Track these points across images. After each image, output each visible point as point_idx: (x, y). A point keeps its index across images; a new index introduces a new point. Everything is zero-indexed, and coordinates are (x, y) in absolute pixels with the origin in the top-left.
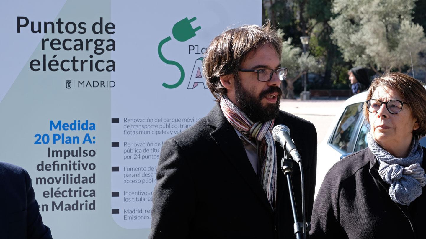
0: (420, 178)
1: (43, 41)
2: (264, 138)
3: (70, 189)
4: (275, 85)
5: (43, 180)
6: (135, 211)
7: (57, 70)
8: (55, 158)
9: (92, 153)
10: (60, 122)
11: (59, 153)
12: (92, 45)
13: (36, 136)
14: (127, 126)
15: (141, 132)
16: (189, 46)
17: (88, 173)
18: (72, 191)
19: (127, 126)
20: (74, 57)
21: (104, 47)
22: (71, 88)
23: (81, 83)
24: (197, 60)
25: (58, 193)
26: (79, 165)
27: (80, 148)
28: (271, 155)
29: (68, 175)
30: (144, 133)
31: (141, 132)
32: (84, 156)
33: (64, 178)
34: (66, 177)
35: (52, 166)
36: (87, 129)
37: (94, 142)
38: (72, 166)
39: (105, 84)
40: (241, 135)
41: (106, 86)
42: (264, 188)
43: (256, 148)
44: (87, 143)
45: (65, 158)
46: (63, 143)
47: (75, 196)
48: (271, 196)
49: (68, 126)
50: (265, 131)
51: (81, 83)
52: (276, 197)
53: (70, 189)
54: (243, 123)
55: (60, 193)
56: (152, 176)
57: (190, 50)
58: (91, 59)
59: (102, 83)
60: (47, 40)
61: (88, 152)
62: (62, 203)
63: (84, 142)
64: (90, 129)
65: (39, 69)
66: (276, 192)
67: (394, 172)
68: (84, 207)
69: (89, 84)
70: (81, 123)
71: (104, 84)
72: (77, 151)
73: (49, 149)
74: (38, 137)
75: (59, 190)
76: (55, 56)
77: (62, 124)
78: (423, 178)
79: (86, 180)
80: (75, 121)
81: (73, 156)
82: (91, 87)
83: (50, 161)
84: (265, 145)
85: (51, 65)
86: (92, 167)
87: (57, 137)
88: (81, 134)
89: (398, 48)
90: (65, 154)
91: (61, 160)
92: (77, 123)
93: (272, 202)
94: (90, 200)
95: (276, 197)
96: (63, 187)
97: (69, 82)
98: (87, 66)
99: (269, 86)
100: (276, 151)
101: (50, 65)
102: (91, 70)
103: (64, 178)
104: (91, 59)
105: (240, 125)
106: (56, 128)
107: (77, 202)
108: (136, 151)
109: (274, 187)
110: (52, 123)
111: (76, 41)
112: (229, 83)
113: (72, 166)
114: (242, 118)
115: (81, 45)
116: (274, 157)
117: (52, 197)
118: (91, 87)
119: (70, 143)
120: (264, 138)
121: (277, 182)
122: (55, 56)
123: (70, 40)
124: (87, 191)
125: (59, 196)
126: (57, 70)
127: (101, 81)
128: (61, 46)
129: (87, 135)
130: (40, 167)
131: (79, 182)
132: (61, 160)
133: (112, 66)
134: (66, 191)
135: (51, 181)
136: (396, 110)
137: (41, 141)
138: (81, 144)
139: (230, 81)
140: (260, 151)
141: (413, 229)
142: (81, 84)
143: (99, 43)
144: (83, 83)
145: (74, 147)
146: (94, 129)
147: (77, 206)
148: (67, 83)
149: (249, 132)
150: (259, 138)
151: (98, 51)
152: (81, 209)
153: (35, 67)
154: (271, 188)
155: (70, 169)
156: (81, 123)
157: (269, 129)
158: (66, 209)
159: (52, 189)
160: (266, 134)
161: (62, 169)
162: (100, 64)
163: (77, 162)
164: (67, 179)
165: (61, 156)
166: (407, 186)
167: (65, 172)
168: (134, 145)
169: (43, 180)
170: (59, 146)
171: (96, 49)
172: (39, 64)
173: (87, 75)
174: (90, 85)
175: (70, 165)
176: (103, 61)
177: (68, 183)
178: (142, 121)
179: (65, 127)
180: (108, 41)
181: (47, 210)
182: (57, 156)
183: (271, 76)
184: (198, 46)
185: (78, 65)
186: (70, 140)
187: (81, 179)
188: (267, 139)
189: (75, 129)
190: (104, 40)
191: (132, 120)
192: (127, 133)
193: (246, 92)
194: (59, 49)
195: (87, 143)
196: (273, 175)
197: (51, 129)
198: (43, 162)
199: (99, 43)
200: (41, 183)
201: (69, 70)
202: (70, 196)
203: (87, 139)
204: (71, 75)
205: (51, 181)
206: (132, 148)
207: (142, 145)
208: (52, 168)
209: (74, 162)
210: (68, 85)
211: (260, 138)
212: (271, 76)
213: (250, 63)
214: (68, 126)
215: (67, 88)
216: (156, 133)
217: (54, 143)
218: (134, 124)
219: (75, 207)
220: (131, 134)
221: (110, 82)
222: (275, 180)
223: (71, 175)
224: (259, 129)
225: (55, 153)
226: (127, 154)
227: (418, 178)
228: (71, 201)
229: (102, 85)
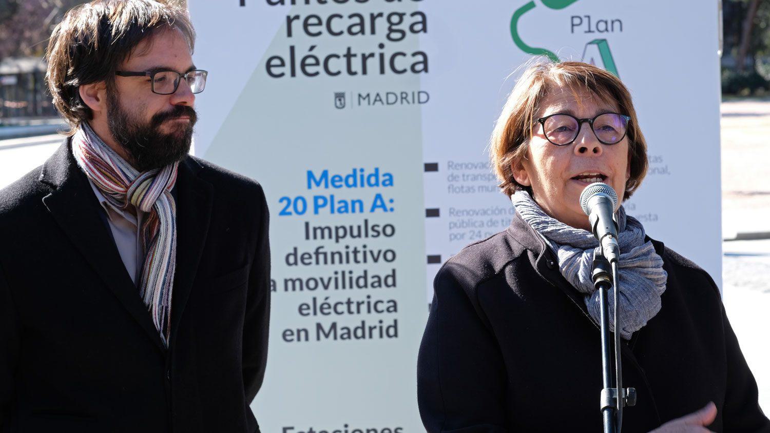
0: (656, 277)
1: (290, 20)
2: (154, 207)
3: (349, 299)
4: (185, 102)
5: (297, 283)
7: (317, 74)
8: (319, 242)
9: (389, 230)
10: (325, 174)
11: (326, 232)
12: (382, 25)
13: (281, 200)
14: (454, 178)
15: (481, 188)
16: (573, 18)
17: (382, 269)
18: (352, 303)
19: (454, 178)
20: (349, 49)
21: (405, 26)
24: (590, 46)
25: (326, 306)
26: (365, 253)
27: (366, 222)
28: (166, 239)
29: (343, 273)
30: (487, 189)
31: (481, 188)
32: (373, 236)
33: (336, 279)
34: (340, 276)
35: (314, 256)
36: (377, 184)
37: (392, 210)
38: (351, 256)
40: (104, 200)
42: (147, 301)
43: (136, 224)
44: (379, 211)
45: (337, 241)
46: (332, 211)
47: (359, 312)
48: (161, 317)
49: (341, 180)
50: (155, 193)
52: (169, 317)
53: (349, 299)
54: (113, 178)
55: (329, 307)
57: (573, 25)
58: (382, 51)
60: (297, 17)
61: (380, 229)
62: (334, 326)
63: (372, 210)
64: (384, 184)
65: (282, 75)
66: (170, 308)
68: (376, 332)
69: (378, 99)
70: (366, 174)
72: (359, 227)
73: (307, 224)
74: (285, 203)
75: (328, 301)
76: (312, 48)
77: (330, 176)
78: (662, 276)
79: (379, 282)
80: (355, 171)
81: (352, 236)
82: (383, 103)
83: (310, 246)
84: (156, 219)
85: (304, 66)
86: (389, 256)
87: (321, 202)
88: (367, 194)
90: (338, 233)
91: (330, 246)
92: (359, 174)
93: (162, 327)
94: (388, 319)
95: (169, 317)
96: (336, 295)
97: (340, 96)
98: (373, 64)
99: (173, 105)
100: (175, 231)
101: (303, 65)
102: (382, 71)
103: (336, 279)
104: (382, 51)
105: (108, 182)
106: (318, 184)
107: (363, 323)
108: (473, 224)
109: (167, 300)
110: (310, 175)
111: (351, 17)
112: (98, 100)
113: (351, 256)
114: (114, 168)
115: (360, 26)
116: (172, 242)
117: (315, 313)
118: (383, 103)
119: (347, 211)
120: (154, 207)
121: (173, 289)
122: (312, 48)
123: (340, 16)
124: (382, 302)
125: (329, 313)
126: (317, 74)
128: (323, 28)
129: (378, 196)
130: (292, 259)
131: (366, 286)
132: (330, 246)
133: (423, 63)
134: (341, 303)
135: (312, 284)
137: (291, 209)
138: (367, 214)
139: (99, 96)
140: (144, 229)
142: (364, 99)
143: (395, 19)
145: (353, 220)
146: (391, 184)
147: (363, 332)
149: (125, 196)
150: (144, 206)
151: (395, 35)
152: (371, 336)
153: (275, 71)
154: (161, 300)
155: (348, 261)
156: (366, 174)
157: (163, 189)
158: (342, 337)
159: (315, 300)
160: (158, 198)
161: (333, 262)
162: (398, 59)
163: (360, 249)
164: (343, 281)
165: (330, 237)
166: (632, 292)
167: (338, 267)
168: (468, 213)
169: (297, 283)
170: (325, 218)
171: (391, 30)
172: (283, 64)
173: (375, 81)
174: (380, 100)
175: (347, 254)
176: (404, 54)
177: (344, 287)
179: (336, 181)
180: (413, 15)
181: (307, 339)
182: (323, 237)
183: (177, 85)
184: (589, 17)
185: (356, 64)
186: (345, 207)
187: (370, 281)
188: (159, 207)
189: (355, 185)
190: (404, 14)
191: (464, 166)
192: (454, 190)
193: (127, 116)
194: (319, 34)
195: (379, 211)
196: (166, 275)
197: (309, 187)
198: (295, 249)
199: (395, 19)
200: (294, 289)
201: (339, 73)
202: (350, 312)
203: (379, 203)
204: (344, 83)
205: (312, 284)
206: (466, 218)
207: (485, 212)
208: (313, 260)
209: (355, 249)
210: (338, 103)
211: (146, 207)
212: (177, 85)
213: (137, 62)
214: (341, 180)
215: (337, 107)
217: (316, 212)
218: (467, 172)
219: (359, 333)
222: (169, 286)
223: (351, 272)
224: (144, 189)
225: (319, 232)
226: (455, 231)
227: (653, 277)
228: (353, 321)
229: (404, 100)
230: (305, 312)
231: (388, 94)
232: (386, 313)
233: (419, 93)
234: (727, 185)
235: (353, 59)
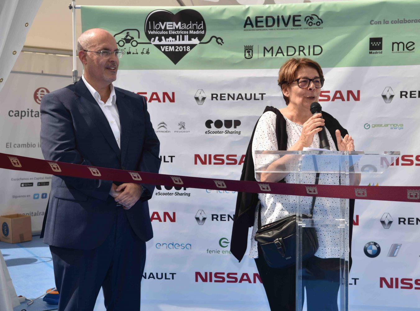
22: (252, 57)
23: (268, 50)
51: (268, 50)
59: (302, 49)
67: (124, 195)
71: (304, 51)
118: (284, 55)
136: (349, 138)
142: (268, 51)
144: (271, 50)
148: (246, 51)
174: (282, 52)
178: (28, 179)
198: (21, 118)
200: (24, 147)
210: (247, 54)
221: (314, 46)
229: (301, 53)
231: (288, 47)
232: (17, 148)
233: (314, 46)
234: (148, 269)
235: (33, 113)
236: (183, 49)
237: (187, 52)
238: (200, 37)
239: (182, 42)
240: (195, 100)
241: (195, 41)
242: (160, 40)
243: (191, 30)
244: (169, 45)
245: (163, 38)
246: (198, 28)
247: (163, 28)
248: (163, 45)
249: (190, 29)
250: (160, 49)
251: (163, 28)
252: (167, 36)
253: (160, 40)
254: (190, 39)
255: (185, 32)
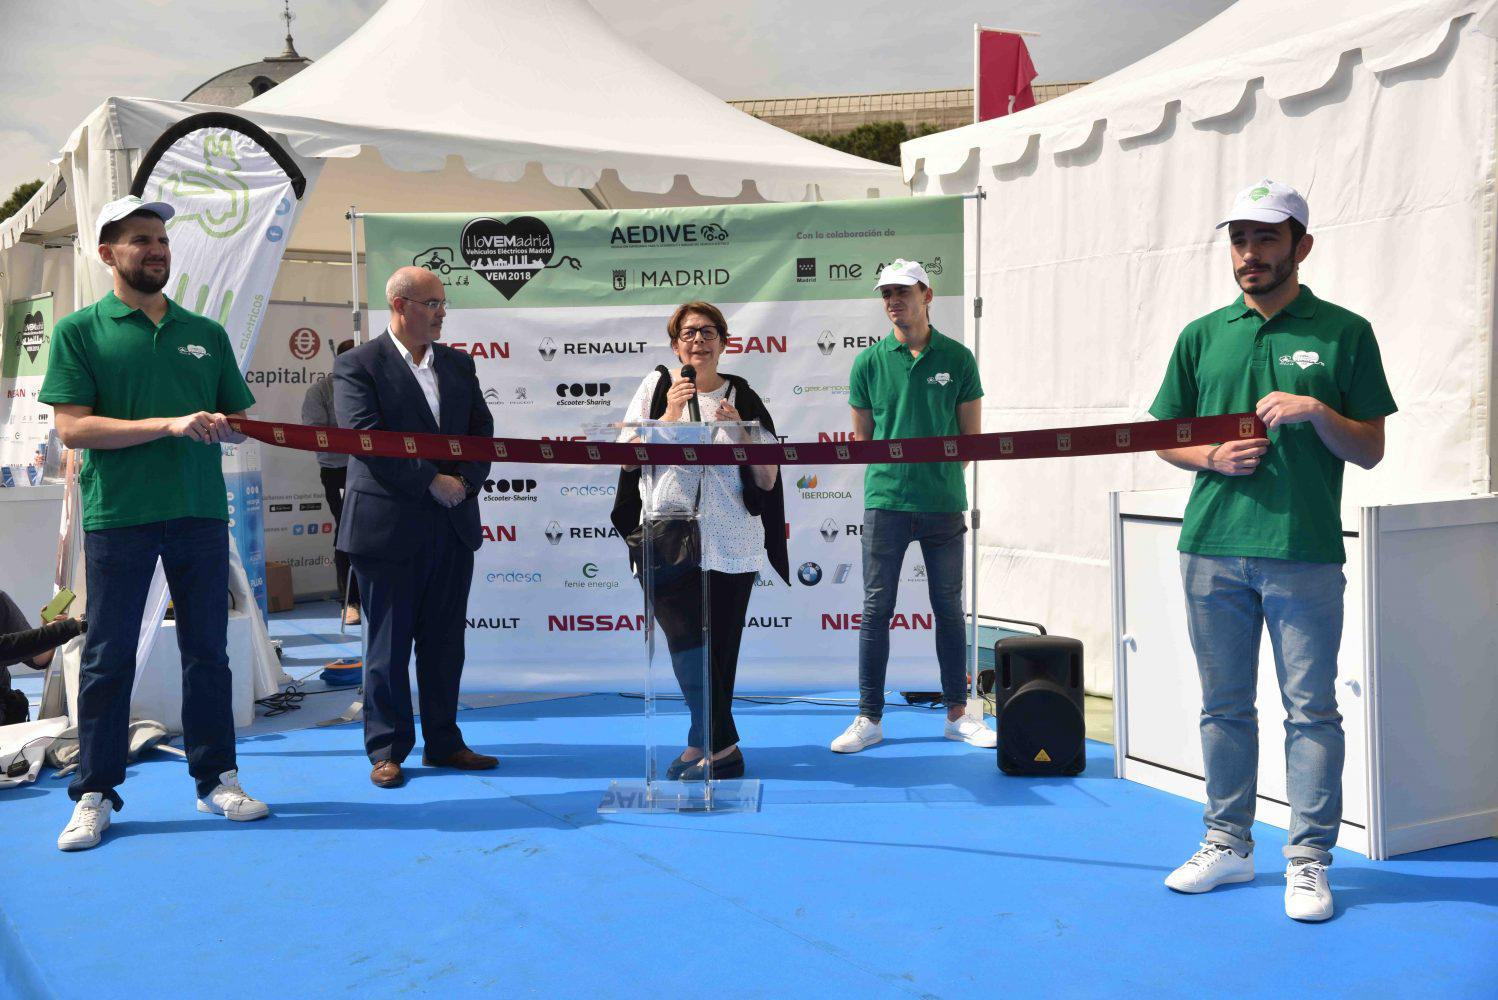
6: (268, 381)
38: (283, 376)
39: (705, 279)
41: (707, 282)
56: (295, 380)
59: (698, 274)
69: (666, 277)
89: (66, 434)
113: (283, 376)
127: (696, 271)
141: (413, 658)
142: (649, 279)
174: (669, 280)
210: (617, 285)
216: (265, 379)
220: (287, 381)
221: (717, 271)
229: (698, 281)
230: (813, 571)
236: (521, 276)
237: (525, 281)
238: (546, 258)
239: (517, 266)
240: (539, 354)
241: (538, 264)
242: (485, 263)
243: (532, 247)
244: (498, 271)
245: (489, 260)
246: (541, 244)
247: (489, 245)
248: (489, 271)
249: (530, 247)
250: (486, 278)
251: (489, 245)
252: (495, 258)
253: (485, 263)
254: (530, 262)
255: (522, 251)
